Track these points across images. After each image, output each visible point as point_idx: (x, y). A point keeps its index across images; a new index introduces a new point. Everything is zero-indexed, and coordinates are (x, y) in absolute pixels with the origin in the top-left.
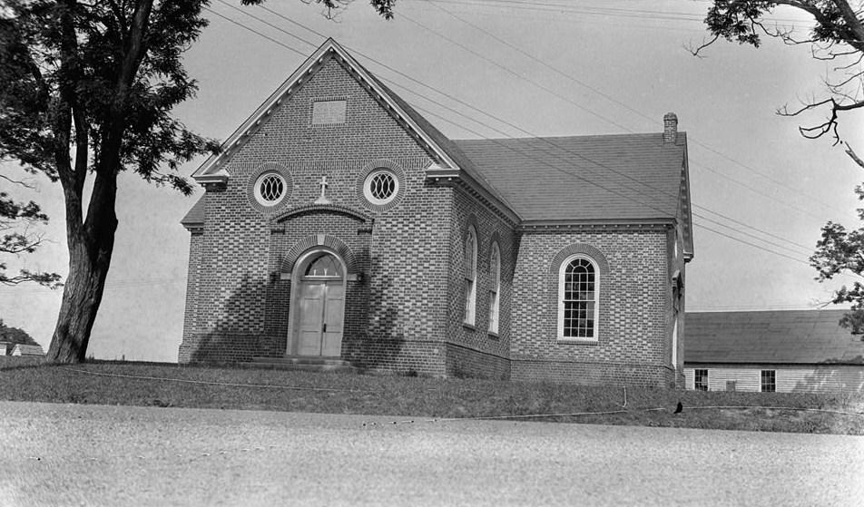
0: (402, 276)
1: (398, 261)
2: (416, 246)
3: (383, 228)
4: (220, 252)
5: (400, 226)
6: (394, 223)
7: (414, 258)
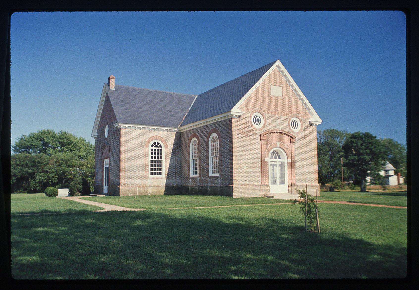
0: (305, 161)
7: (308, 154)
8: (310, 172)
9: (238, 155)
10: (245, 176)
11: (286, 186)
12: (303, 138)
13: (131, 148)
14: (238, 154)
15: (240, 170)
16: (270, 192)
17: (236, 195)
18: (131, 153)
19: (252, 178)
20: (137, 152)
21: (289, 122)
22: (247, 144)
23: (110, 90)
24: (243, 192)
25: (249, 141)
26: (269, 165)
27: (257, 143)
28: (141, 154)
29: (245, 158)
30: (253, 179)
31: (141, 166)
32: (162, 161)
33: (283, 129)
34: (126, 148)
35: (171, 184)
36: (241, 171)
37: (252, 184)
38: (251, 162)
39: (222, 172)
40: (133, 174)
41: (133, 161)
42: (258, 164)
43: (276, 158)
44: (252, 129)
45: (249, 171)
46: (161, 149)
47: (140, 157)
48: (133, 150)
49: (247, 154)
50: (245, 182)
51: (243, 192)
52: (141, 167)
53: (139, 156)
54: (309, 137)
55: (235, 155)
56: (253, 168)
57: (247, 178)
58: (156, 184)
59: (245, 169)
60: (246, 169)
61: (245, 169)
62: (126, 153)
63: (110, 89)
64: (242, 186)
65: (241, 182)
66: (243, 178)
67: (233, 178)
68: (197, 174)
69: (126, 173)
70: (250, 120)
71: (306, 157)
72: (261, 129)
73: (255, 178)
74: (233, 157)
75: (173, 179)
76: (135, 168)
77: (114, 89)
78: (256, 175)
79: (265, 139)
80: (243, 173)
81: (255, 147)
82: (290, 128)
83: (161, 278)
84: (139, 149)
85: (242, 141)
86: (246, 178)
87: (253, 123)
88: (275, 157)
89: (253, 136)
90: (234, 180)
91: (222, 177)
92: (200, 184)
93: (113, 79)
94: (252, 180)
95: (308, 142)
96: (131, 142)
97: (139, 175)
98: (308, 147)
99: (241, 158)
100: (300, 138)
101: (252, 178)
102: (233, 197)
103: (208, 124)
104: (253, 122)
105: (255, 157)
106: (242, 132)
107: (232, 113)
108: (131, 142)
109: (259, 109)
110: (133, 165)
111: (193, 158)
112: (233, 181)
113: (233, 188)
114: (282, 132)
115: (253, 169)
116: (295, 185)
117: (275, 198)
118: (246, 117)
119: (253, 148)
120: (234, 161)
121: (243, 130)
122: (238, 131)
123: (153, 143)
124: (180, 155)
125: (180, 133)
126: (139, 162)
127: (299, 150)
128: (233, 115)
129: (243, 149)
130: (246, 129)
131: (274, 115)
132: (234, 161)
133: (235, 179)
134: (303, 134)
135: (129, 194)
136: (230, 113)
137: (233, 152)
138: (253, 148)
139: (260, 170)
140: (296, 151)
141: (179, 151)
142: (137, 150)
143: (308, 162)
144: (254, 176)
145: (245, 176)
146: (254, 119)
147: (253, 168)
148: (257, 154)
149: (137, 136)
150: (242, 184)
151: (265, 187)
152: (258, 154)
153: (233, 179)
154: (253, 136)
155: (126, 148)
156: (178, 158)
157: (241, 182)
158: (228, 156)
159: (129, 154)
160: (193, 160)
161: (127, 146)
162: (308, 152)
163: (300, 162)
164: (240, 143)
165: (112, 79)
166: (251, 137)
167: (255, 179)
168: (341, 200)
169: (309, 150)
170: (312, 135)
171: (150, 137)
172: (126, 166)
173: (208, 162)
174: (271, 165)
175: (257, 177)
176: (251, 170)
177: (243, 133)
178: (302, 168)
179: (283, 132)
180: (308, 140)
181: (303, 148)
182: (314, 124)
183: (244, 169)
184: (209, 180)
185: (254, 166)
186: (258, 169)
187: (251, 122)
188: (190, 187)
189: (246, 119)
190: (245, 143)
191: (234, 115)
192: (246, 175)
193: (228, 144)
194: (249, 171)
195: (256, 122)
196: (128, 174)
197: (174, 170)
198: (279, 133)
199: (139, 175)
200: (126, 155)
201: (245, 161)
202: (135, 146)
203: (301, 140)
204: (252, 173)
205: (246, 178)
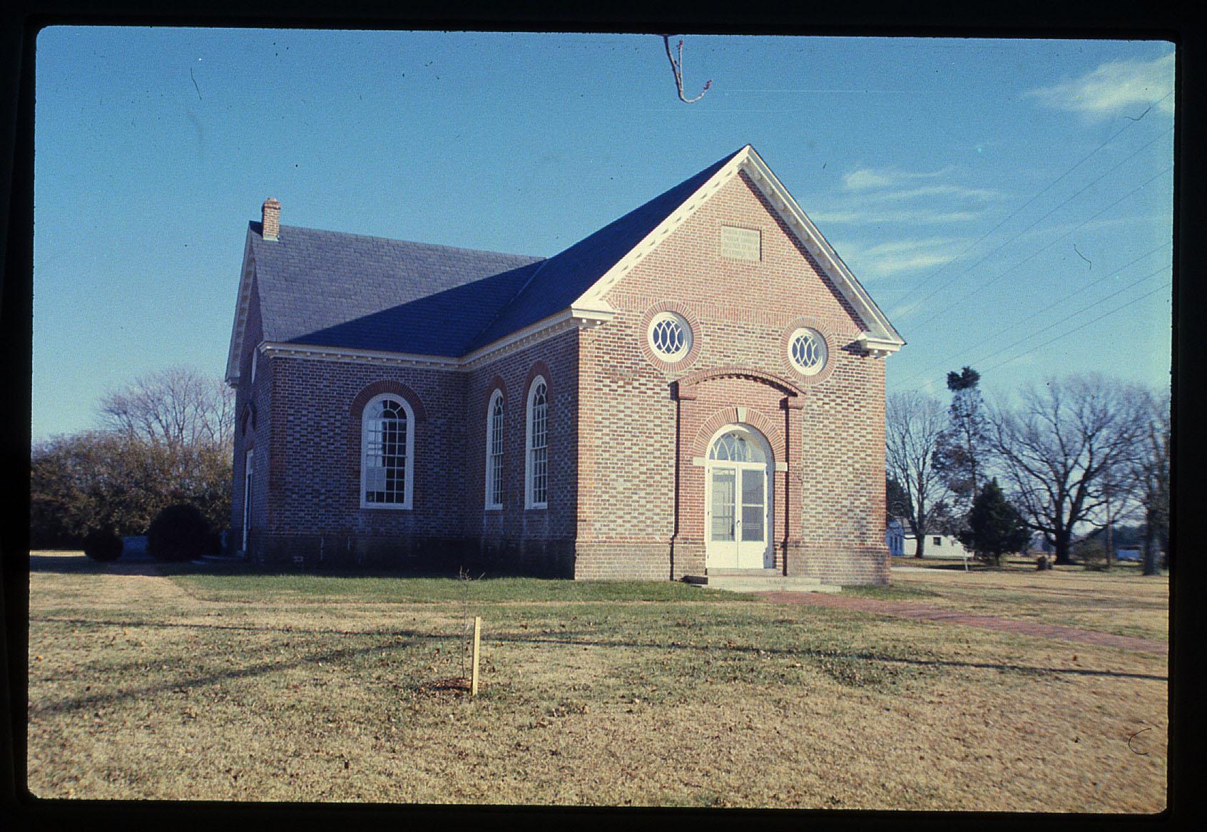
0: (838, 469)
7: (850, 447)
8: (857, 507)
10: (620, 513)
11: (760, 547)
13: (304, 419)
14: (598, 442)
17: (585, 569)
19: (642, 518)
21: (785, 343)
22: (628, 412)
23: (263, 241)
25: (637, 400)
26: (708, 478)
27: (665, 410)
29: (621, 456)
30: (648, 522)
31: (336, 474)
32: (406, 460)
33: (762, 364)
36: (606, 497)
37: (644, 538)
38: (644, 469)
39: (553, 497)
40: (309, 497)
41: (310, 456)
42: (665, 474)
47: (333, 444)
48: (311, 423)
49: (628, 444)
50: (620, 530)
51: (608, 563)
54: (858, 392)
55: (585, 446)
56: (650, 486)
57: (627, 517)
60: (624, 489)
61: (621, 489)
62: (290, 432)
63: (265, 238)
64: (605, 542)
65: (605, 529)
66: (612, 517)
68: (544, 501)
71: (845, 458)
72: (680, 365)
73: (656, 518)
75: (440, 515)
76: (317, 480)
77: (277, 240)
78: (657, 510)
79: (694, 395)
80: (612, 501)
81: (657, 422)
82: (787, 363)
85: (614, 403)
86: (621, 517)
90: (579, 523)
91: (552, 513)
94: (642, 526)
95: (851, 409)
97: (330, 501)
99: (606, 455)
102: (573, 578)
104: (795, 355)
105: (657, 454)
107: (575, 314)
109: (677, 301)
112: (576, 525)
115: (650, 490)
116: (796, 546)
119: (650, 425)
120: (582, 463)
121: (616, 366)
123: (402, 409)
124: (463, 442)
125: (466, 374)
127: (819, 433)
128: (580, 320)
129: (614, 427)
130: (629, 363)
132: (582, 463)
134: (833, 382)
137: (579, 435)
138: (650, 425)
139: (673, 494)
141: (463, 429)
144: (649, 514)
145: (620, 513)
146: (798, 347)
148: (666, 442)
151: (687, 548)
152: (667, 443)
153: (577, 521)
154: (651, 385)
156: (457, 451)
157: (605, 529)
159: (298, 436)
161: (292, 411)
163: (820, 471)
164: (606, 406)
165: (270, 208)
166: (643, 388)
168: (954, 590)
169: (857, 436)
170: (869, 385)
174: (717, 478)
175: (662, 516)
181: (833, 426)
182: (876, 352)
183: (615, 489)
184: (525, 522)
186: (665, 490)
187: (645, 342)
189: (629, 331)
190: (622, 407)
191: (584, 321)
195: (802, 356)
198: (747, 377)
199: (330, 501)
200: (289, 439)
201: (619, 465)
202: (318, 413)
203: (827, 400)
205: (621, 517)
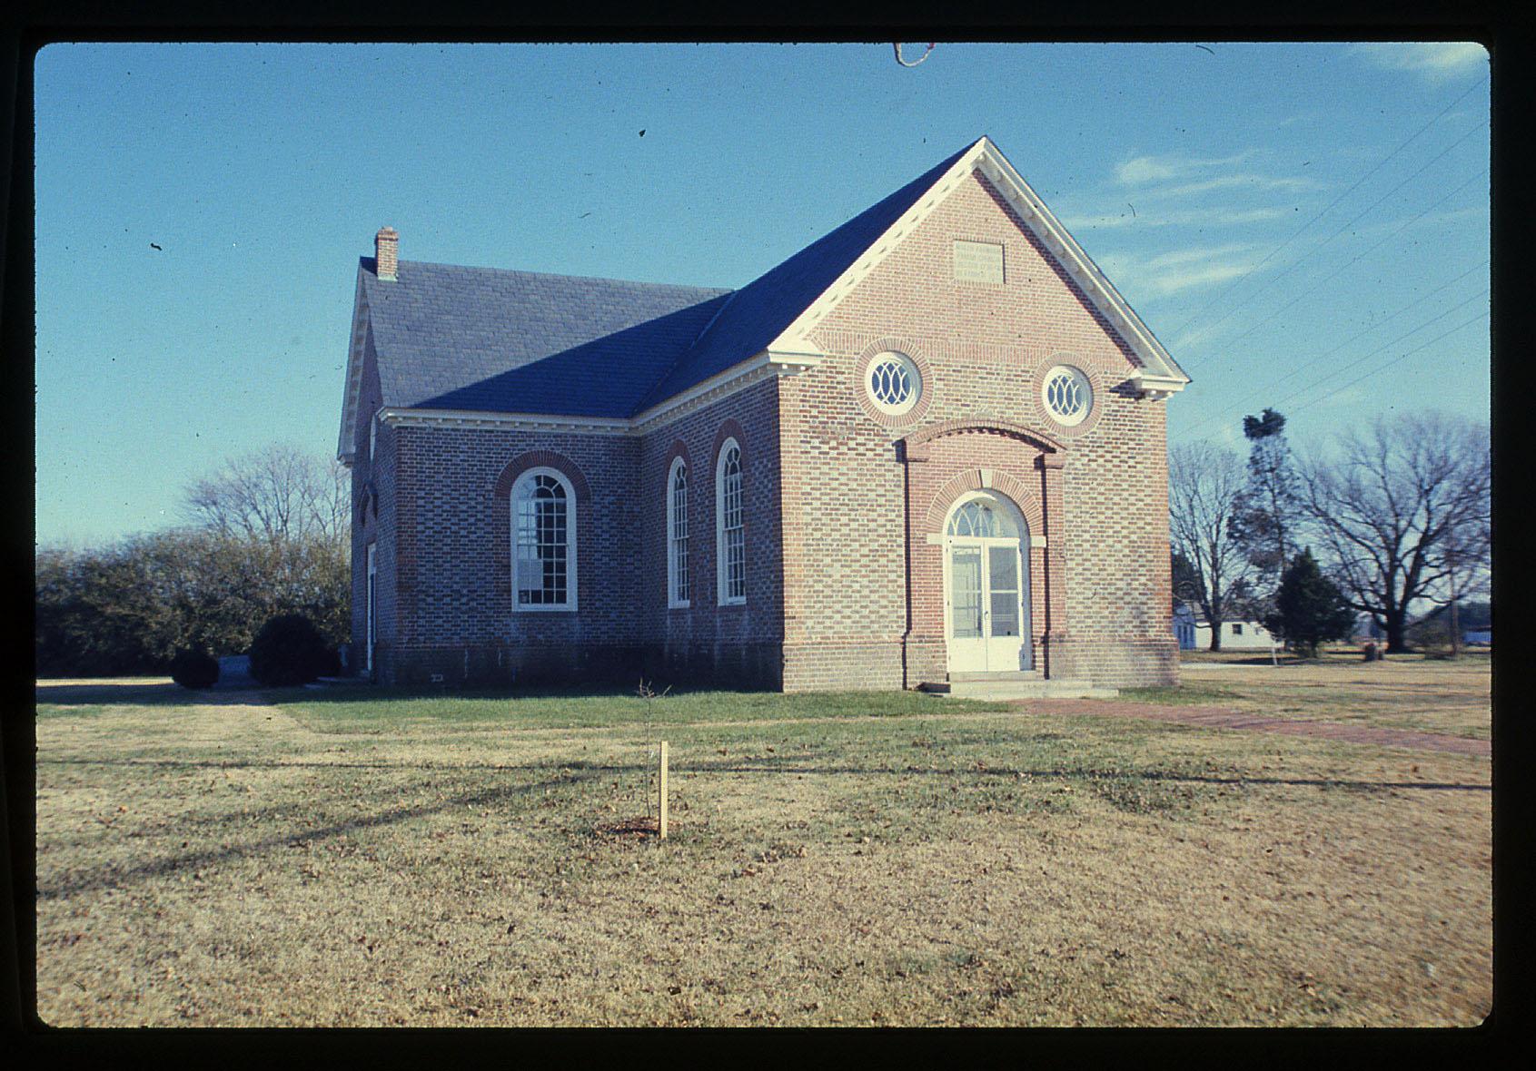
0: (1110, 541)
1: (1102, 517)
2: (1125, 494)
3: (1078, 465)
4: (817, 494)
5: (1101, 461)
6: (1093, 456)
7: (1124, 514)
9: (806, 524)
10: (838, 607)
11: (1016, 643)
12: (1101, 451)
14: (808, 519)
15: (816, 581)
16: (948, 671)
17: (797, 678)
18: (438, 519)
19: (866, 612)
20: (463, 516)
21: (1039, 385)
22: (843, 479)
23: (378, 281)
24: (824, 670)
25: (854, 464)
27: (889, 476)
28: (481, 525)
29: (836, 535)
30: (873, 617)
34: (421, 502)
35: (605, 637)
36: (819, 587)
38: (865, 551)
41: (446, 549)
42: (892, 556)
43: (953, 534)
44: (867, 416)
45: (856, 586)
46: (561, 500)
48: (446, 507)
50: (838, 628)
52: (481, 574)
53: (473, 529)
54: (1132, 444)
56: (874, 571)
57: (847, 612)
58: (540, 636)
59: (837, 576)
60: (842, 576)
61: (837, 576)
63: (380, 278)
66: (828, 612)
67: (783, 612)
68: (742, 594)
69: (422, 596)
70: (861, 378)
73: (883, 612)
74: (784, 532)
75: (613, 616)
77: (395, 280)
78: (884, 602)
80: (828, 592)
82: (1042, 410)
83: (800, 1026)
84: (473, 503)
85: (825, 469)
87: (872, 395)
88: (959, 530)
89: (871, 445)
92: (694, 636)
93: (391, 240)
94: (865, 622)
95: (1125, 467)
96: (440, 477)
97: (473, 604)
98: (1125, 486)
99: (817, 535)
100: (1086, 450)
101: (866, 612)
103: (713, 401)
105: (882, 531)
106: (822, 432)
107: (773, 359)
108: (440, 477)
110: (447, 566)
111: (727, 526)
113: (785, 653)
114: (1001, 427)
115: (874, 576)
116: (1061, 641)
117: (957, 691)
118: (843, 373)
119: (872, 495)
122: (806, 427)
125: (638, 439)
126: (471, 554)
129: (826, 499)
131: (967, 361)
133: (794, 618)
135: (433, 676)
136: (768, 357)
138: (872, 495)
140: (1067, 502)
142: (464, 507)
143: (1126, 547)
144: (874, 607)
145: (838, 607)
146: (1056, 391)
147: (874, 571)
148: (892, 516)
149: (462, 456)
150: (822, 638)
151: (923, 648)
153: (783, 618)
154: (871, 445)
155: (421, 502)
157: (819, 628)
158: (768, 526)
159: (431, 524)
160: (727, 535)
161: (422, 494)
162: (1124, 504)
163: (1086, 545)
164: (816, 473)
165: (385, 239)
166: (861, 450)
167: (882, 616)
171: (515, 456)
172: (423, 570)
173: (715, 551)
174: (957, 559)
175: (890, 609)
176: (865, 581)
177: (826, 437)
178: (1096, 570)
179: (1008, 428)
180: (1124, 457)
183: (830, 576)
185: (876, 564)
186: (893, 576)
188: (667, 647)
189: (840, 378)
190: (835, 474)
191: (785, 367)
192: (841, 602)
193: (769, 481)
194: (856, 586)
196: (430, 600)
197: (615, 584)
198: (992, 431)
199: (473, 604)
200: (420, 528)
201: (834, 547)
203: (1093, 456)
204: (865, 592)
